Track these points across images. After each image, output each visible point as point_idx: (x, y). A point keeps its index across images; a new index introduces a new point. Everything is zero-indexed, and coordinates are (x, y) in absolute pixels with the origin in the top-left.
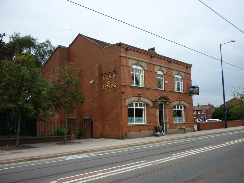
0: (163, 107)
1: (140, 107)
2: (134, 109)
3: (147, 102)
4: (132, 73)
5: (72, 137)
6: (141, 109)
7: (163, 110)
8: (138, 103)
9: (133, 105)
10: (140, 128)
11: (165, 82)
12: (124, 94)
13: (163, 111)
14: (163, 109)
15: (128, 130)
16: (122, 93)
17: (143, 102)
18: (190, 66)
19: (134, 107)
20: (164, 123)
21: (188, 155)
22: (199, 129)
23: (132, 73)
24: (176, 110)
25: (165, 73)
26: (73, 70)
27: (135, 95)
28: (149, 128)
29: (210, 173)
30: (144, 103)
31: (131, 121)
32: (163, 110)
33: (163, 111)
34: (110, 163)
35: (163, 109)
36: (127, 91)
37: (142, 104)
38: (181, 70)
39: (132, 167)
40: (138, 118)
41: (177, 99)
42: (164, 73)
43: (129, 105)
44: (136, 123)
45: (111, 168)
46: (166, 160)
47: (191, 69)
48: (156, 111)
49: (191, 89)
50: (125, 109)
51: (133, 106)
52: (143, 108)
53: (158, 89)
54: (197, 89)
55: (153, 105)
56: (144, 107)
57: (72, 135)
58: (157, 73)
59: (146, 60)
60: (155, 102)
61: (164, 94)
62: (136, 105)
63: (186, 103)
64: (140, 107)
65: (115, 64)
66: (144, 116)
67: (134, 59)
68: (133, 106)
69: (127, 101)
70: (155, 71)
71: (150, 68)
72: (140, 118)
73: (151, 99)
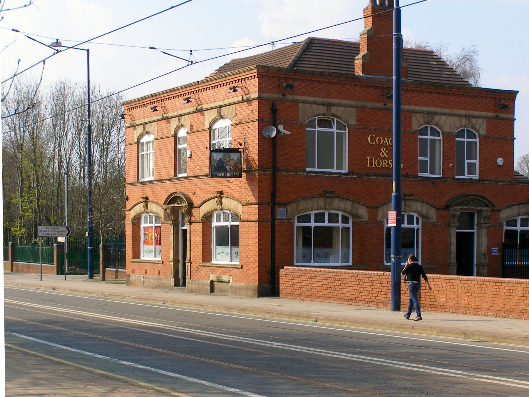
0: (476, 222)
1: (408, 224)
4: (420, 158)
6: (330, 230)
7: (475, 231)
8: (323, 214)
9: (516, 222)
10: (146, 268)
13: (473, 233)
14: (473, 229)
17: (415, 212)
18: (511, 95)
19: (313, 224)
23: (420, 158)
26: (75, 169)
28: (159, 269)
33: (473, 233)
35: (476, 227)
38: (183, 112)
40: (320, 251)
43: (507, 222)
45: (224, 345)
47: (516, 102)
51: (516, 226)
62: (320, 218)
63: (235, 203)
64: (408, 224)
68: (516, 226)
72: (327, 250)
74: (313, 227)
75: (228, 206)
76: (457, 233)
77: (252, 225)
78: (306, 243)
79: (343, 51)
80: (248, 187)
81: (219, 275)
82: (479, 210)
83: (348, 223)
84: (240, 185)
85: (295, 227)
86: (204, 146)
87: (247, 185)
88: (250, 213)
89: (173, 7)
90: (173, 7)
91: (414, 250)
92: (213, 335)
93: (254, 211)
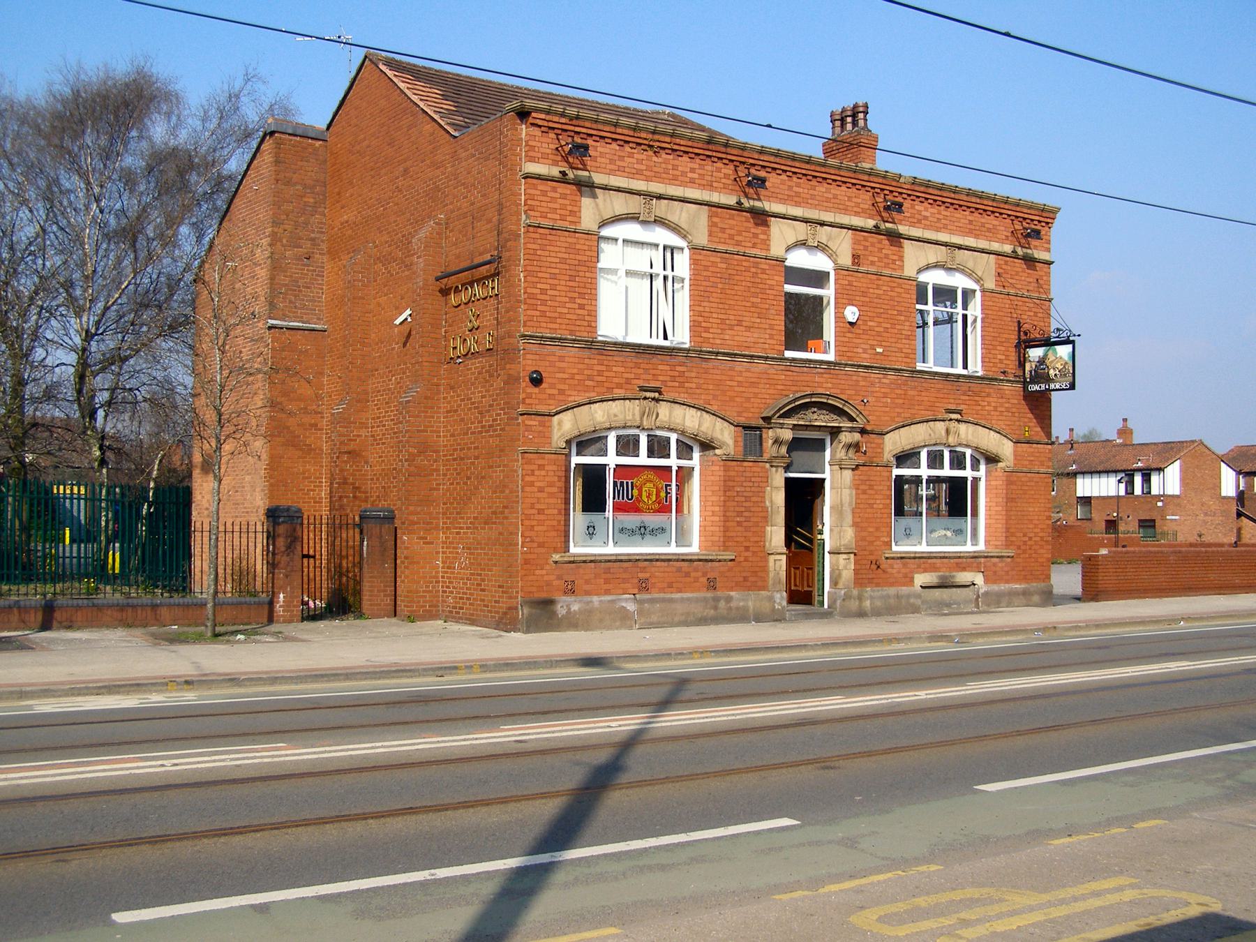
2: (966, 478)
3: (703, 429)
5: (279, 608)
11: (840, 317)
12: (544, 385)
15: (704, 580)
16: (525, 383)
18: (1047, 215)
19: (924, 472)
20: (827, 548)
21: (713, 719)
22: (1092, 592)
24: (669, 468)
25: (846, 261)
27: (619, 393)
28: (710, 575)
29: (332, 832)
30: (976, 449)
31: (591, 531)
32: (827, 475)
34: (315, 733)
35: (827, 467)
36: (562, 371)
37: (964, 454)
39: (154, 763)
41: (731, 414)
42: (835, 262)
44: (615, 543)
46: (443, 742)
48: (766, 479)
49: (1035, 353)
50: (541, 467)
52: (968, 473)
53: (789, 354)
54: (1064, 351)
55: (745, 446)
56: (975, 467)
57: (281, 596)
58: (787, 263)
59: (710, 186)
60: (759, 428)
61: (824, 386)
62: (627, 445)
65: (500, 222)
66: (975, 514)
67: (618, 190)
69: (560, 423)
70: (902, 267)
71: (731, 237)
73: (728, 415)
74: (925, 478)
75: (976, 440)
76: (788, 480)
77: (1038, 480)
78: (593, 502)
79: (486, 106)
80: (1028, 411)
81: (947, 574)
82: (835, 430)
83: (691, 459)
84: (1007, 405)
85: (573, 466)
86: (858, 331)
87: (1026, 407)
88: (1032, 458)
89: (769, 126)
90: (769, 126)
91: (966, 521)
92: (495, 737)
93: (1042, 455)
